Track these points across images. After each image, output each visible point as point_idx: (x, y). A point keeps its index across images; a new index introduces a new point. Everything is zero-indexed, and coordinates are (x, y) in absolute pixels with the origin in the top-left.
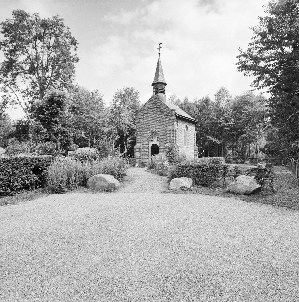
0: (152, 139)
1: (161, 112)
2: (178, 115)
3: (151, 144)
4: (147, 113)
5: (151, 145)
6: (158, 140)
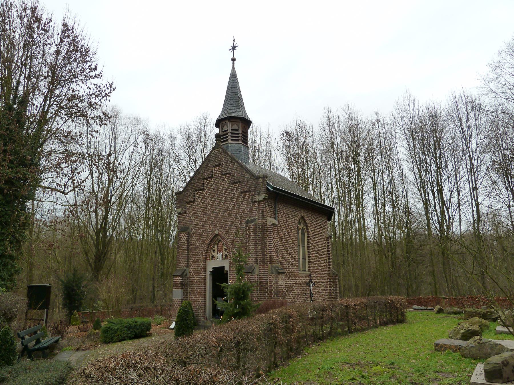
0: (213, 254)
1: (232, 184)
2: (273, 188)
3: (211, 266)
4: (203, 189)
5: (211, 270)
6: (226, 255)
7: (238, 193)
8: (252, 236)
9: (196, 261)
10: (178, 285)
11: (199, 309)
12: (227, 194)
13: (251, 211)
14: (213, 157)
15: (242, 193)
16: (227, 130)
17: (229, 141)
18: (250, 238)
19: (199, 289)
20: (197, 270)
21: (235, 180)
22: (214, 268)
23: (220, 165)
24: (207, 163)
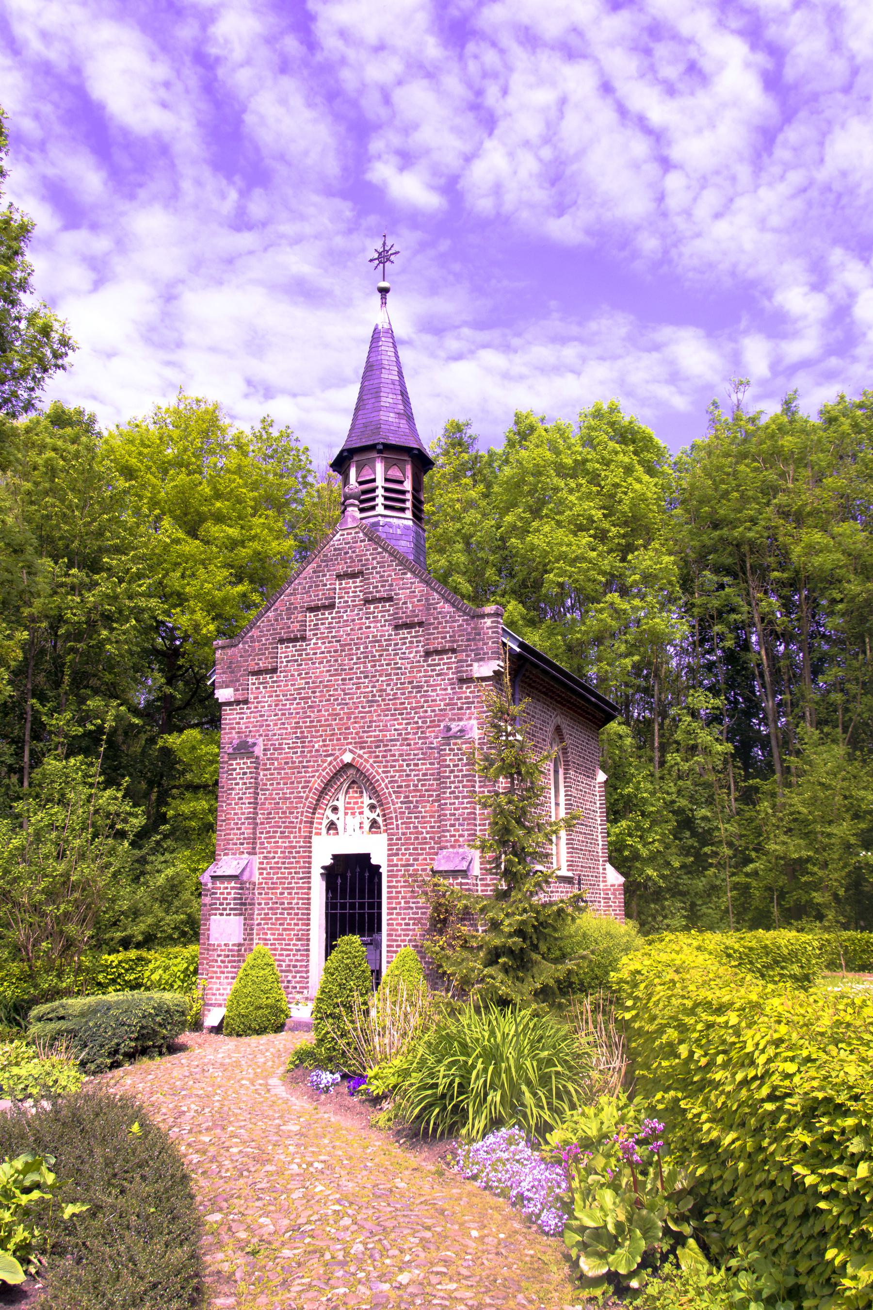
0: (333, 817)
1: (397, 627)
4: (304, 639)
5: (328, 862)
7: (415, 653)
8: (461, 771)
9: (280, 838)
10: (228, 904)
11: (290, 971)
12: (381, 656)
13: (456, 704)
14: (335, 550)
15: (428, 654)
16: (374, 480)
17: (380, 510)
18: (455, 777)
19: (289, 914)
20: (284, 863)
21: (407, 617)
22: (335, 857)
23: (361, 573)
24: (320, 566)
